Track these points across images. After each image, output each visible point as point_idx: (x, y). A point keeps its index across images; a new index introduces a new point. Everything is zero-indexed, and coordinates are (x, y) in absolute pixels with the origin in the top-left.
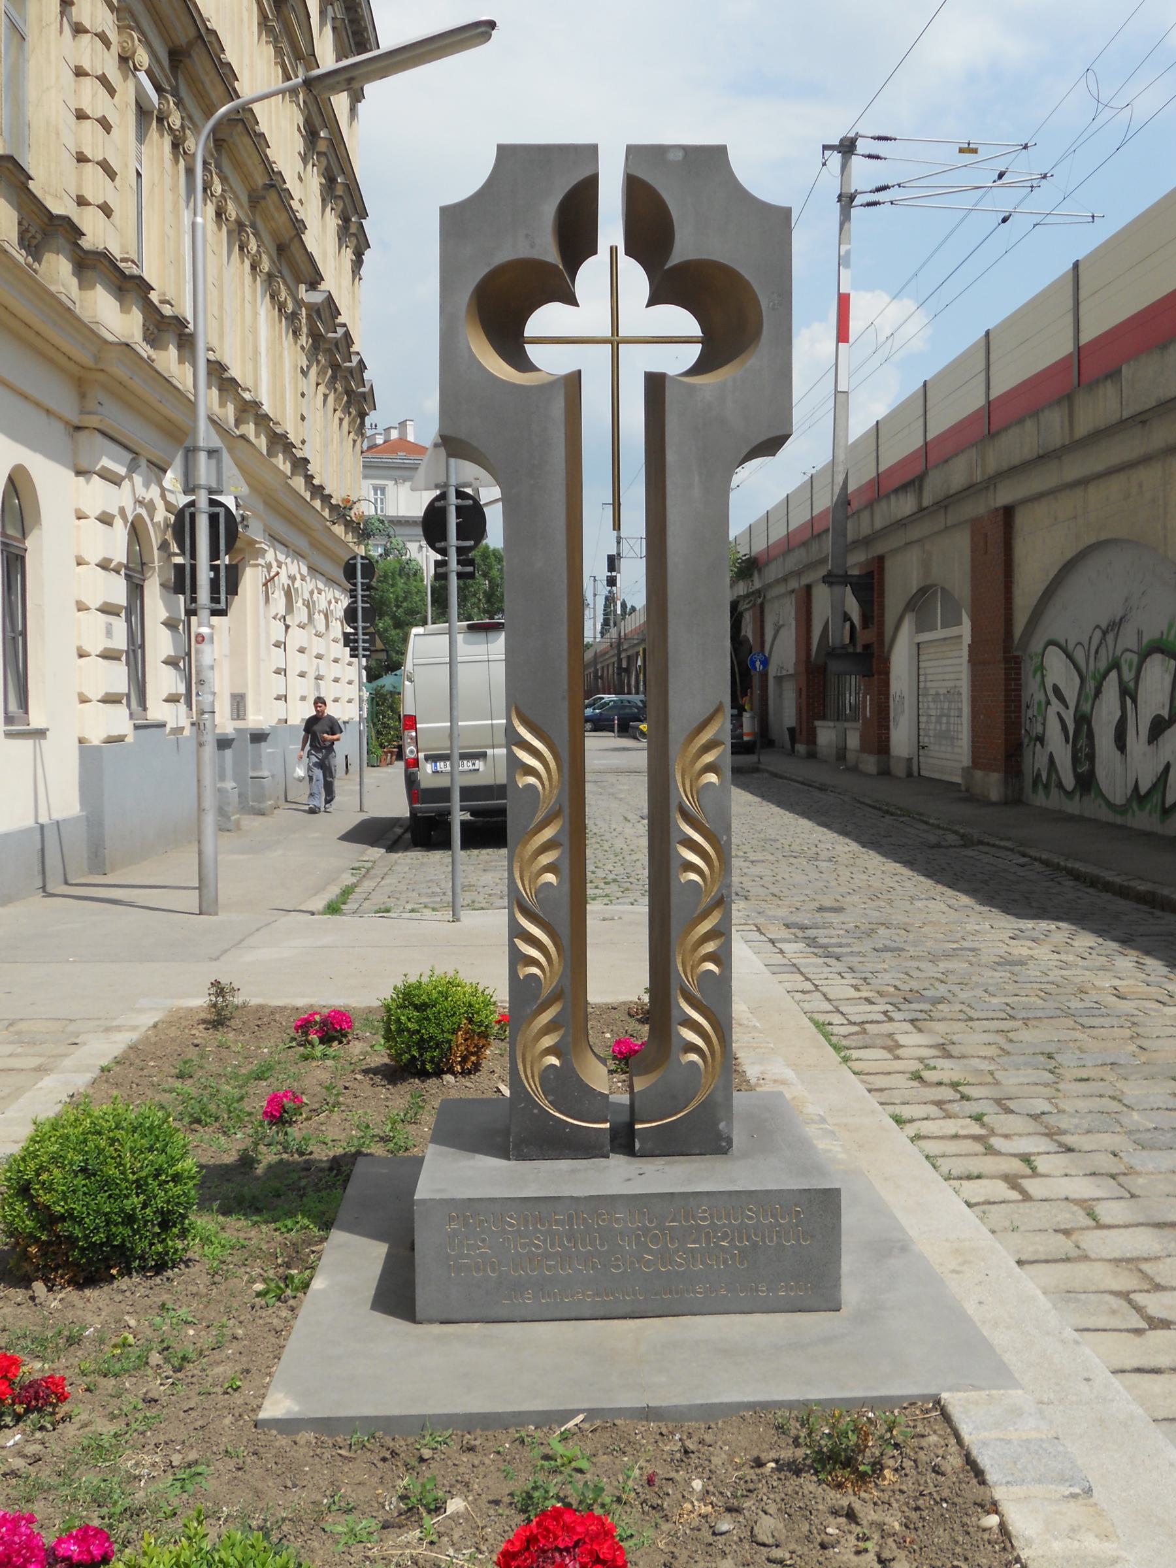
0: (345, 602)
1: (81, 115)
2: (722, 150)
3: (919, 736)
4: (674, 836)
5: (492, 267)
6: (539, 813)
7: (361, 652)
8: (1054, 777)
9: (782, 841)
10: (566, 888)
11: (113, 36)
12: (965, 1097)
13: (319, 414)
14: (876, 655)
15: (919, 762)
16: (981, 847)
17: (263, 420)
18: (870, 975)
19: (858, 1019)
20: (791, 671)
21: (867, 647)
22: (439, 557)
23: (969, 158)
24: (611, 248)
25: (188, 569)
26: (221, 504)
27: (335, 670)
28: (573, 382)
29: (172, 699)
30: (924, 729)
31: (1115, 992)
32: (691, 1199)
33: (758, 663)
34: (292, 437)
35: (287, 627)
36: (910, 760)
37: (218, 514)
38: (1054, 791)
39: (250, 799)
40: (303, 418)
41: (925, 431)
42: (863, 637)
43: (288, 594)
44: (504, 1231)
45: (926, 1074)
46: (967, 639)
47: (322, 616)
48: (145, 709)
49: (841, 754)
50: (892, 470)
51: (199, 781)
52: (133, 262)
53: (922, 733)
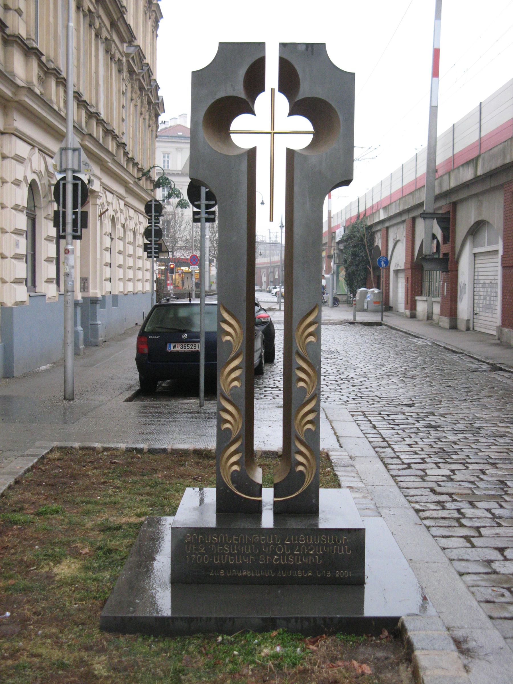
3: (474, 307)
4: (294, 366)
5: (215, 100)
6: (232, 354)
7: (153, 255)
9: (387, 366)
10: (244, 388)
14: (450, 260)
15: (473, 322)
16: (500, 372)
17: (100, 122)
20: (403, 267)
21: (446, 255)
22: (196, 210)
26: (79, 179)
28: (252, 153)
30: (477, 303)
33: (383, 263)
34: (116, 132)
35: (112, 239)
36: (468, 321)
37: (78, 184)
39: (90, 337)
41: (480, 131)
42: (444, 249)
43: (113, 220)
46: (501, 253)
47: (132, 232)
49: (429, 317)
50: (462, 153)
51: (65, 328)
52: (33, 40)
53: (475, 305)
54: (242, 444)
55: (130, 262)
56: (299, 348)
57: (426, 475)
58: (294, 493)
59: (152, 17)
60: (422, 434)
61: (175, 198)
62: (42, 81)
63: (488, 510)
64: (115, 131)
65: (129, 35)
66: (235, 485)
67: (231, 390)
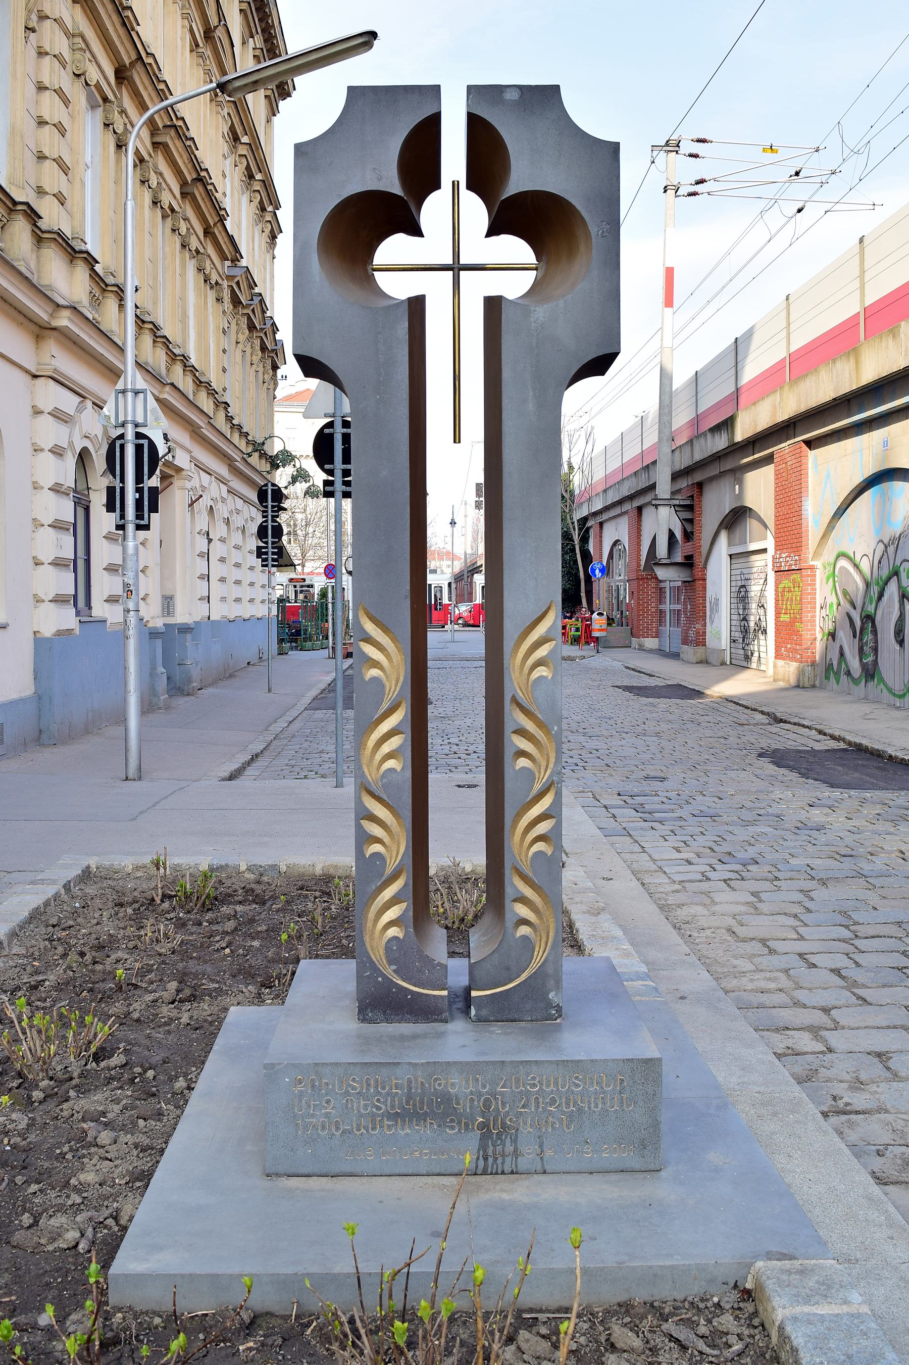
0: (260, 520)
1: (42, 123)
2: (557, 87)
4: (509, 727)
7: (270, 562)
8: (843, 666)
10: (408, 774)
11: (67, 55)
12: (772, 952)
13: (239, 367)
18: (689, 838)
19: (678, 878)
23: (770, 157)
24: (453, 182)
25: (118, 490)
26: (144, 437)
27: (249, 576)
28: (417, 306)
29: (112, 600)
31: (902, 856)
32: (521, 1067)
33: (597, 571)
35: (210, 541)
38: (844, 678)
40: (224, 370)
44: (347, 1093)
45: (738, 929)
48: (90, 608)
54: (406, 885)
55: (236, 574)
56: (519, 691)
57: (714, 903)
58: (511, 981)
59: (265, 230)
60: (691, 828)
61: (301, 483)
62: (96, 302)
63: (837, 972)
64: (212, 384)
65: (231, 249)
66: (394, 967)
67: (383, 776)
